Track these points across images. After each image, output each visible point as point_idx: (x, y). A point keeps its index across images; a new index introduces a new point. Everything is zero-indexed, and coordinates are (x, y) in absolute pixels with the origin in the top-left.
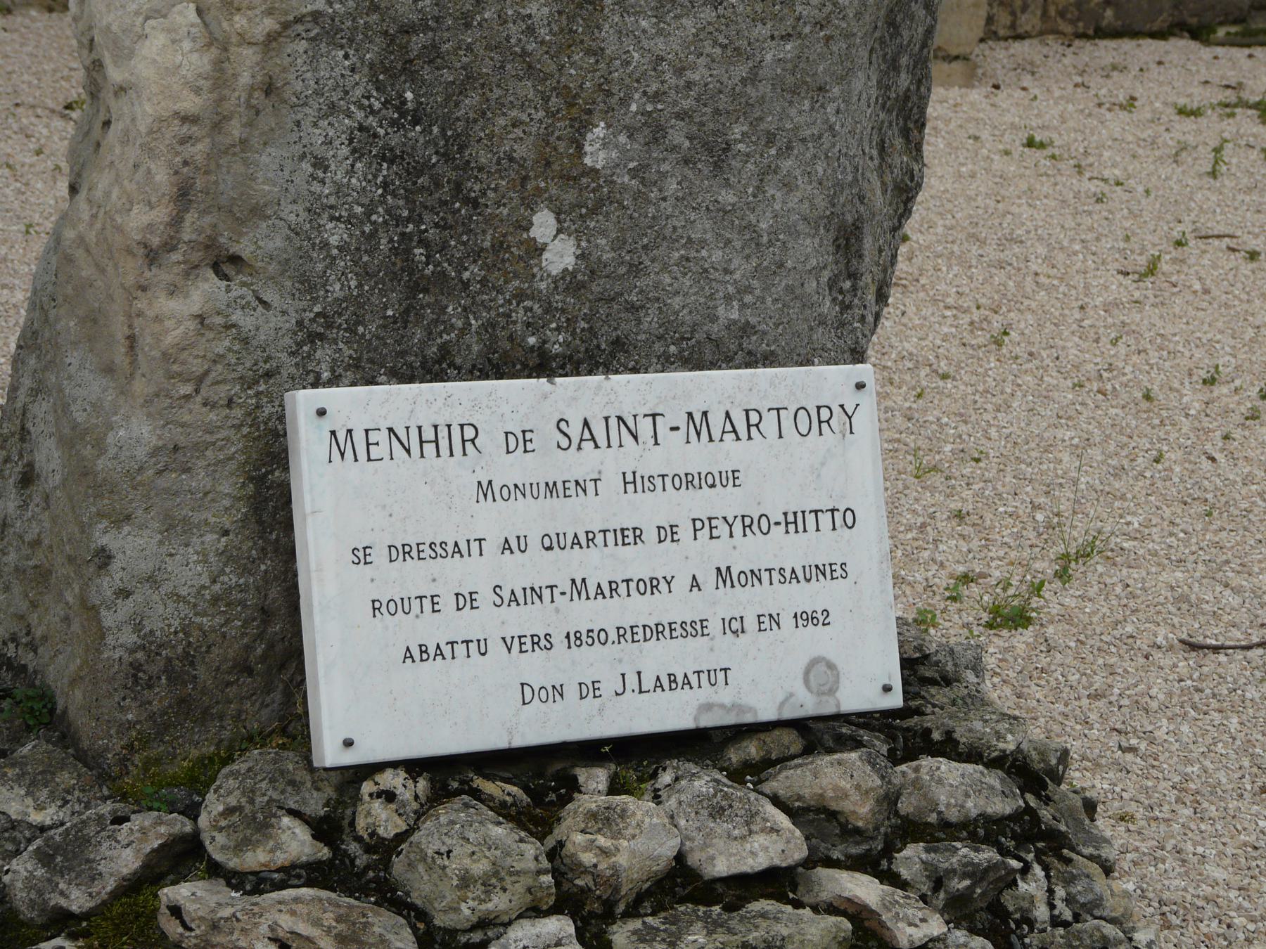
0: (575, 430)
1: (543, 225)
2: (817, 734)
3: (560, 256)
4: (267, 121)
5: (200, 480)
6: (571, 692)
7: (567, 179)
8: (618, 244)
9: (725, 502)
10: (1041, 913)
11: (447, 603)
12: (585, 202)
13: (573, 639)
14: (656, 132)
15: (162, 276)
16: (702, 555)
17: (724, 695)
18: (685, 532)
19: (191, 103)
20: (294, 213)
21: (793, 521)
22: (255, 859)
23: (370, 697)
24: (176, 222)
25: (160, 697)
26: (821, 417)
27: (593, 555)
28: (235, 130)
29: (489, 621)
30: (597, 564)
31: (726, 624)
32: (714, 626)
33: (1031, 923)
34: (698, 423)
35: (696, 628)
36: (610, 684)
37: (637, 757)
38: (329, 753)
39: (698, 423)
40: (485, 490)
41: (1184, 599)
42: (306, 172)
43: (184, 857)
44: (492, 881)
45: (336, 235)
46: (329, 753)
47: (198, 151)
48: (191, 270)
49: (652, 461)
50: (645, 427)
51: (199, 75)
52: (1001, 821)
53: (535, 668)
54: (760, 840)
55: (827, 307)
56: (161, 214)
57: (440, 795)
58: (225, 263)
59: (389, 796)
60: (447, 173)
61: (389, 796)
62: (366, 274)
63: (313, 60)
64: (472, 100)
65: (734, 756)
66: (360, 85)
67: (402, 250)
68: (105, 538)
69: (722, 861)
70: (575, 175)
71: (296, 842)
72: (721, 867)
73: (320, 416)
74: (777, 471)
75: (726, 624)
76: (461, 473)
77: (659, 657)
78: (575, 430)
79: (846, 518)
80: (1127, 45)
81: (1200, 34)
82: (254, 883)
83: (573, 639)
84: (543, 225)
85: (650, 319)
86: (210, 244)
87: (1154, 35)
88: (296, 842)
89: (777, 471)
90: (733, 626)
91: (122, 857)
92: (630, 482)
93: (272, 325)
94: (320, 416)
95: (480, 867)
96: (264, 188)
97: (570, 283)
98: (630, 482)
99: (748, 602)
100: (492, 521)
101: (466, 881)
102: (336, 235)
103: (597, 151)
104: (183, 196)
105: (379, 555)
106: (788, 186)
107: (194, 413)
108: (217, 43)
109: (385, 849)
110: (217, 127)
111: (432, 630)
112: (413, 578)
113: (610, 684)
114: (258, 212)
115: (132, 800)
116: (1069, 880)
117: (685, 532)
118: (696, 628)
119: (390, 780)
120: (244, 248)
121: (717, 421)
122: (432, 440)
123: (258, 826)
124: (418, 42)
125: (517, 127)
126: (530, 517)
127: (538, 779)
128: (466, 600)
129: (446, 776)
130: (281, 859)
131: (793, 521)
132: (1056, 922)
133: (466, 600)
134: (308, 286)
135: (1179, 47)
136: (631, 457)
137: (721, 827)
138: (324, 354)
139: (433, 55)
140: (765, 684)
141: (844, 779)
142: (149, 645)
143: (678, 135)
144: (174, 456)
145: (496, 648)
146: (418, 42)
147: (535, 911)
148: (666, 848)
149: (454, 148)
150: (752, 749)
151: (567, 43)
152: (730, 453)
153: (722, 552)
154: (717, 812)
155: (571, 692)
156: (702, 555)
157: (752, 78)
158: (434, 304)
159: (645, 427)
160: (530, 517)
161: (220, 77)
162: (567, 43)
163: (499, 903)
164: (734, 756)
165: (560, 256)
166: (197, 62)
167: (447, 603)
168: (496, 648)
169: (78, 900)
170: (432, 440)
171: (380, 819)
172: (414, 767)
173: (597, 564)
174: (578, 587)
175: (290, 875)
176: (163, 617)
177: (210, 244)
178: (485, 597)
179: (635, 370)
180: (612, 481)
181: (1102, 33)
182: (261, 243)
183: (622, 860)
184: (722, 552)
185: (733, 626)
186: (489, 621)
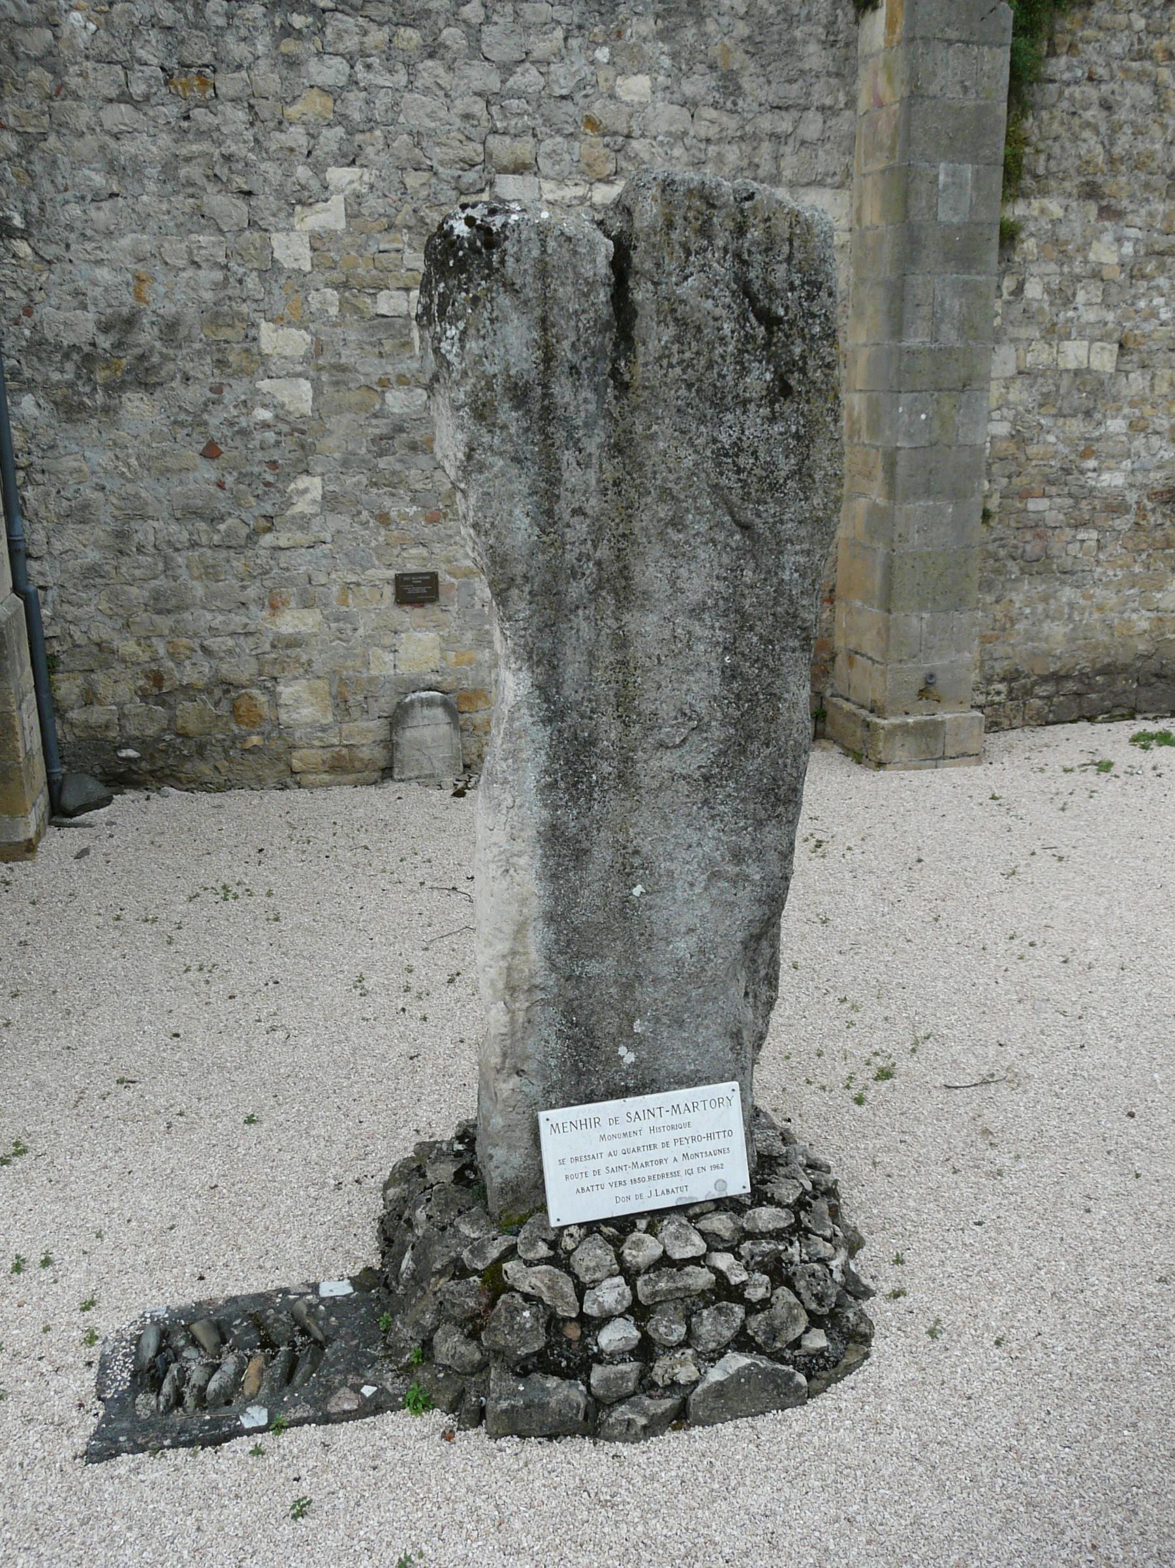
0: (633, 1115)
1: (622, 1050)
2: (721, 1204)
3: (629, 1058)
4: (530, 1030)
5: (518, 1134)
6: (633, 1198)
7: (628, 1037)
8: (649, 1053)
9: (687, 1132)
10: (797, 1259)
11: (590, 1174)
12: (635, 1042)
13: (633, 1181)
14: (657, 1020)
15: (501, 1077)
16: (677, 1150)
17: (686, 1194)
18: (672, 1144)
19: (504, 1030)
20: (539, 1057)
21: (710, 1136)
22: (531, 1256)
23: (566, 1206)
24: (503, 1062)
25: (509, 1198)
26: (719, 1101)
27: (639, 1154)
28: (519, 1035)
29: (605, 1178)
30: (641, 1157)
31: (687, 1172)
32: (682, 1173)
33: (791, 1263)
34: (675, 1109)
35: (676, 1174)
36: (646, 1194)
37: (656, 1218)
38: (554, 1223)
39: (675, 1109)
40: (603, 1138)
41: (954, 1061)
42: (544, 1044)
43: (510, 1253)
44: (596, 1268)
45: (553, 1062)
46: (554, 1223)
47: (508, 1042)
48: (509, 1075)
49: (659, 1122)
50: (657, 1112)
51: (387, 1186)
52: (783, 1230)
53: (621, 1191)
54: (689, 1248)
55: (730, 1056)
56: (499, 1060)
57: (589, 1233)
58: (519, 1072)
59: (571, 1235)
60: (588, 1040)
61: (571, 1235)
62: (564, 1072)
63: (543, 1012)
64: (594, 1018)
65: (691, 1212)
66: (559, 1017)
67: (575, 1064)
68: (491, 1151)
69: (678, 1254)
70: (631, 1035)
71: (543, 1250)
72: (677, 1256)
73: (548, 1118)
74: (702, 1122)
75: (687, 1172)
76: (595, 1133)
77: (662, 1184)
78: (633, 1115)
79: (730, 1133)
80: (1060, 726)
81: (1091, 719)
82: (529, 1264)
83: (633, 1181)
84: (622, 1050)
85: (663, 1072)
86: (515, 1067)
87: (1071, 722)
88: (543, 1250)
89: (702, 1122)
90: (689, 1172)
91: (494, 1253)
92: (652, 1130)
93: (535, 1089)
94: (548, 1118)
95: (592, 1264)
96: (530, 1051)
97: (634, 1065)
98: (652, 1130)
99: (694, 1164)
100: (605, 1147)
101: (587, 1269)
102: (553, 1062)
103: (638, 1027)
104: (505, 1055)
105: (567, 1162)
106: (707, 1027)
107: (513, 1116)
108: (511, 1012)
109: (570, 1253)
110: (513, 1034)
111: (585, 1183)
112: (580, 1167)
113: (646, 1194)
114: (528, 1057)
115: (502, 1232)
116: (808, 1246)
117: (672, 1144)
118: (676, 1174)
119: (573, 1230)
120: (525, 1068)
121: (682, 1107)
122: (585, 1124)
123: (532, 1245)
124: (576, 1003)
125: (611, 1023)
126: (618, 1145)
127: (621, 1227)
128: (597, 1172)
129: (591, 1228)
130: (538, 1256)
131: (710, 1136)
132: (802, 1261)
133: (597, 1172)
134: (545, 1078)
135: (1084, 724)
136: (652, 1122)
137: (678, 1243)
138: (553, 1097)
139: (581, 1007)
140: (701, 1190)
141: (721, 1224)
142: (506, 1182)
143: (665, 1020)
144: (509, 1127)
145: (607, 1186)
146: (576, 1003)
147: (612, 1275)
148: (658, 1252)
149: (590, 1032)
150: (697, 1210)
151: (624, 998)
152: (687, 1117)
153: (684, 1149)
154: (677, 1238)
155: (633, 1198)
156: (677, 1150)
157: (689, 1001)
158: (588, 1074)
159: (657, 1112)
160: (618, 1145)
161: (513, 1021)
162: (624, 998)
163: (598, 1275)
164: (691, 1212)
165: (629, 1058)
166: (505, 1019)
167: (590, 1174)
168: (607, 1186)
169: (480, 1266)
170: (585, 1124)
171: (568, 1243)
172: (580, 1225)
173: (641, 1157)
174: (635, 1165)
175: (540, 1261)
176: (510, 1174)
177: (515, 1067)
178: (603, 1171)
179: (659, 1091)
180: (646, 1131)
181: (1048, 724)
182: (530, 1066)
183: (639, 1260)
184: (684, 1149)
185: (689, 1172)
186: (605, 1178)
